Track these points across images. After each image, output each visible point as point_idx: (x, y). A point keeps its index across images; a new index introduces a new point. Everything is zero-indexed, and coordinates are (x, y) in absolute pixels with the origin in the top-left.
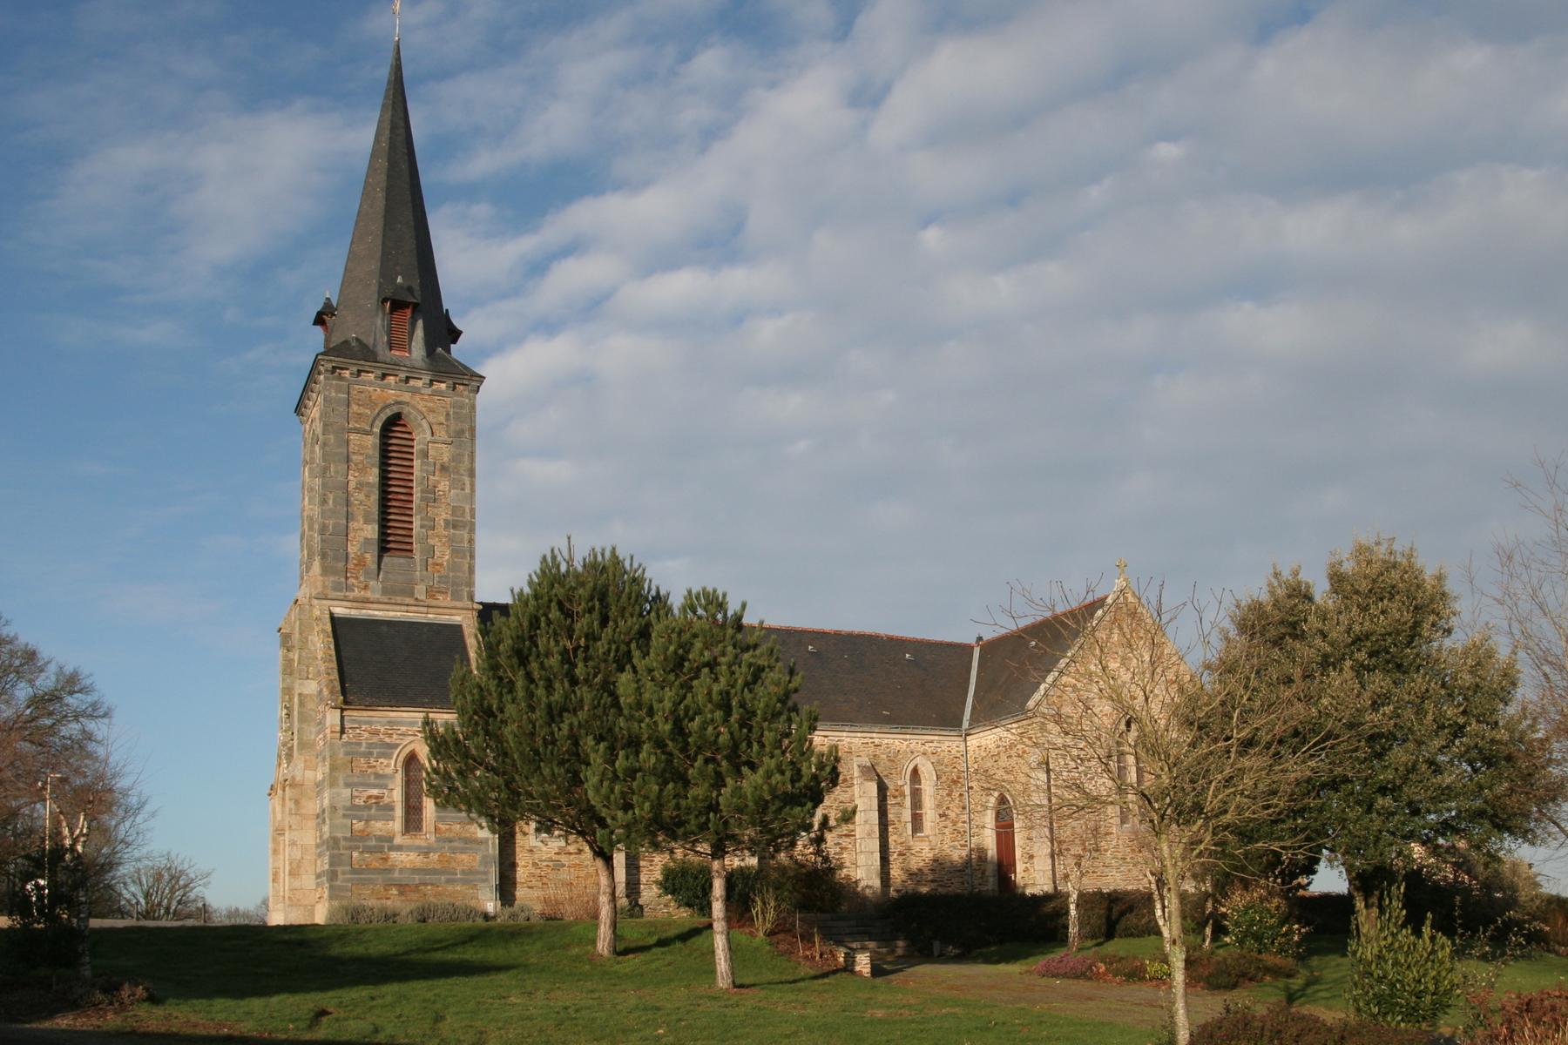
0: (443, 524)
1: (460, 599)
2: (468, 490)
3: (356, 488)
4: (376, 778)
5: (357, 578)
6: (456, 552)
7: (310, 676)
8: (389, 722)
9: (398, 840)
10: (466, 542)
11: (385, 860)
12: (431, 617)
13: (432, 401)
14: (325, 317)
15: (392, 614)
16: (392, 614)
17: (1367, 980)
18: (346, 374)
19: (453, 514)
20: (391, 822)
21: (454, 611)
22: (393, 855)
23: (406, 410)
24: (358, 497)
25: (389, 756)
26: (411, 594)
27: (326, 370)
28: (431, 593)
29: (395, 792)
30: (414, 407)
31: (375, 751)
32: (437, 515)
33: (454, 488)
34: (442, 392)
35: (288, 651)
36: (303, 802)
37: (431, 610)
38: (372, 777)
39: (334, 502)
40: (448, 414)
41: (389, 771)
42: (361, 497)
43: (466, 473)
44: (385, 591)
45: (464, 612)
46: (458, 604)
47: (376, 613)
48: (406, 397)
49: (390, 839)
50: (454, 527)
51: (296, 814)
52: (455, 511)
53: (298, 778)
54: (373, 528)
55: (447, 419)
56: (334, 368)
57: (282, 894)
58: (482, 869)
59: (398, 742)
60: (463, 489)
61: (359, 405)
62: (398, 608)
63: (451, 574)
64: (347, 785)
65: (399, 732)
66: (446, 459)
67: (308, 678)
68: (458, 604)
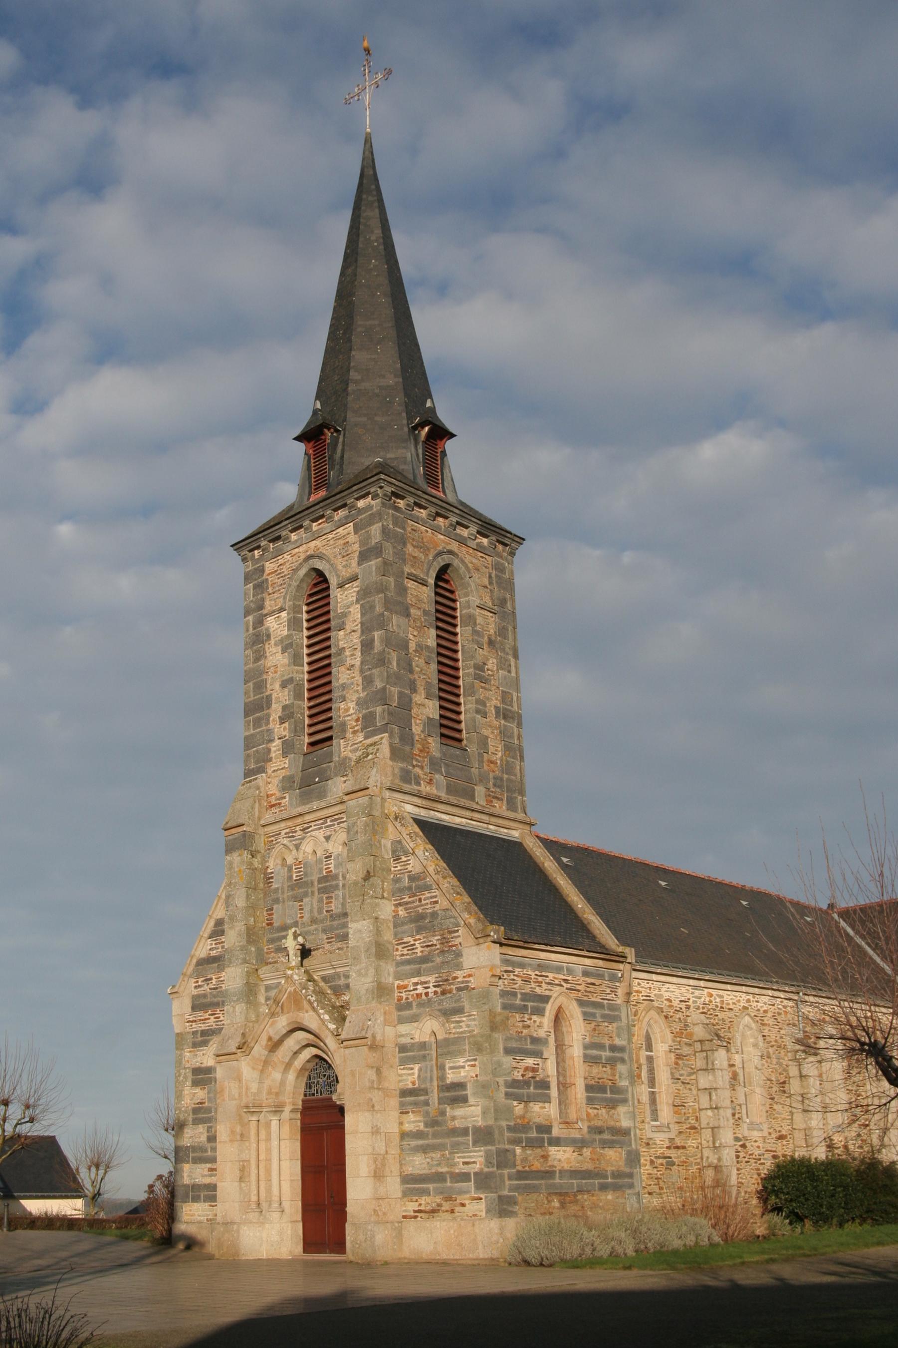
0: (494, 712)
1: (515, 810)
2: (513, 674)
3: (416, 651)
4: (532, 1043)
5: (422, 768)
6: (508, 748)
7: (385, 895)
8: (539, 965)
9: (556, 1132)
10: (516, 738)
11: (545, 1157)
12: (491, 829)
13: (475, 557)
14: (326, 431)
15: (458, 820)
16: (458, 820)
17: (147, 1219)
18: (401, 504)
19: (503, 701)
20: (547, 1105)
21: (512, 824)
22: (553, 1150)
23: (456, 562)
24: (418, 662)
25: (540, 1012)
26: (472, 798)
27: (385, 495)
28: (491, 797)
29: (549, 1061)
30: (463, 562)
31: (530, 1004)
32: (488, 699)
33: (502, 669)
34: (484, 547)
35: (253, 856)
36: (385, 1072)
37: (493, 820)
38: (529, 1041)
39: (398, 664)
40: (490, 577)
41: (541, 1033)
42: (422, 662)
43: (511, 652)
44: (450, 790)
45: (521, 826)
46: (512, 815)
47: (444, 817)
48: (454, 546)
49: (547, 1129)
50: (505, 717)
51: (378, 1089)
52: (505, 697)
53: (379, 1037)
54: (434, 704)
55: (491, 583)
56: (393, 493)
57: (254, 1198)
58: (627, 1170)
59: (547, 993)
60: (509, 672)
61: (415, 547)
62: (468, 814)
63: (505, 776)
64: (508, 1051)
65: (548, 980)
66: (492, 632)
67: (383, 897)
68: (512, 815)
